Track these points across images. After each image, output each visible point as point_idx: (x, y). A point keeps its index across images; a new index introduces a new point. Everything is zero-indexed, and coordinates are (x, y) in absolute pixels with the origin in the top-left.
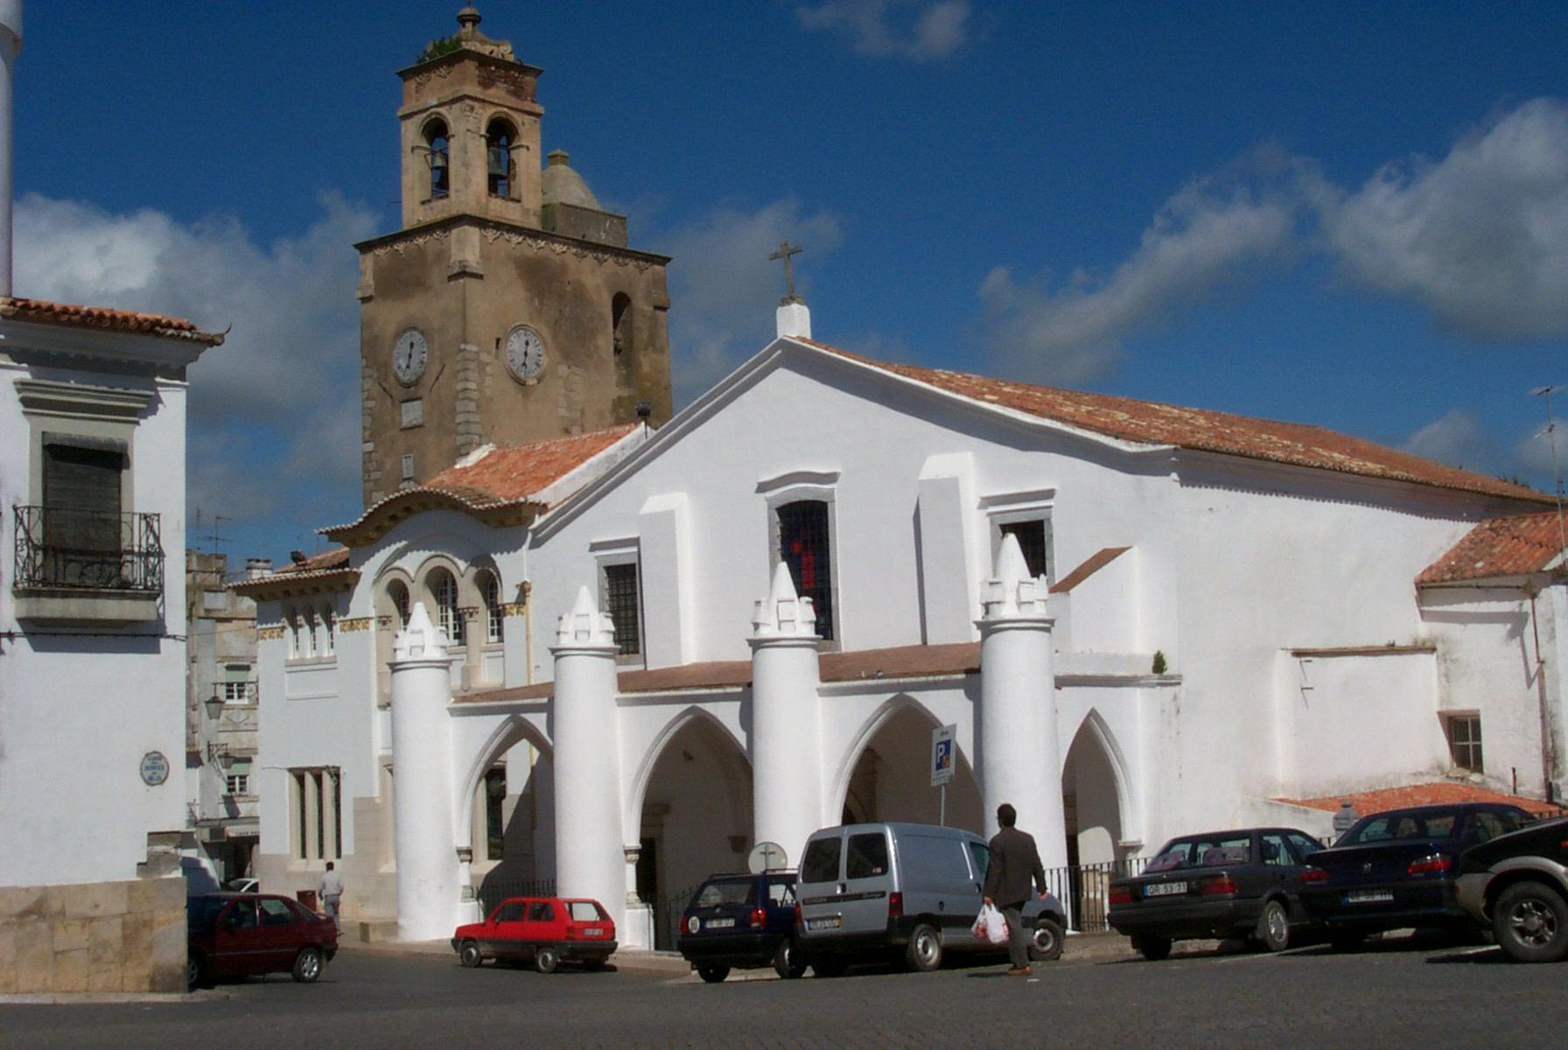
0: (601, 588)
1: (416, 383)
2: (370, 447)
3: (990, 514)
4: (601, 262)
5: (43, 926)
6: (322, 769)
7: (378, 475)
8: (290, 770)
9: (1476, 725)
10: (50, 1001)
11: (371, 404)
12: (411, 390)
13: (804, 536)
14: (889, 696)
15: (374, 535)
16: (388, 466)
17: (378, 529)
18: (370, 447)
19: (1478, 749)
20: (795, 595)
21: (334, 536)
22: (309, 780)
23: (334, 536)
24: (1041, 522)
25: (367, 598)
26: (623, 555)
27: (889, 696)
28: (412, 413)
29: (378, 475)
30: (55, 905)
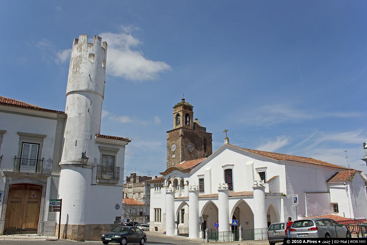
0: (343, 167)
1: (174, 152)
2: (168, 161)
3: (257, 171)
4: (202, 134)
5: (98, 230)
6: (156, 208)
7: (169, 165)
8: (154, 208)
9: (337, 205)
10: (37, 240)
11: (168, 155)
12: (174, 153)
13: (228, 174)
14: (208, 201)
15: (167, 174)
16: (170, 164)
17: (167, 173)
18: (168, 161)
19: (338, 209)
20: (225, 183)
21: (161, 174)
22: (157, 210)
23: (161, 174)
24: (203, 179)
25: (166, 183)
26: (201, 177)
27: (208, 201)
28: (174, 156)
29: (169, 165)
30: (100, 227)
